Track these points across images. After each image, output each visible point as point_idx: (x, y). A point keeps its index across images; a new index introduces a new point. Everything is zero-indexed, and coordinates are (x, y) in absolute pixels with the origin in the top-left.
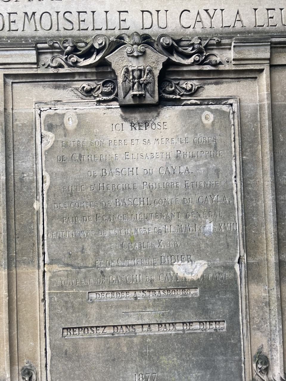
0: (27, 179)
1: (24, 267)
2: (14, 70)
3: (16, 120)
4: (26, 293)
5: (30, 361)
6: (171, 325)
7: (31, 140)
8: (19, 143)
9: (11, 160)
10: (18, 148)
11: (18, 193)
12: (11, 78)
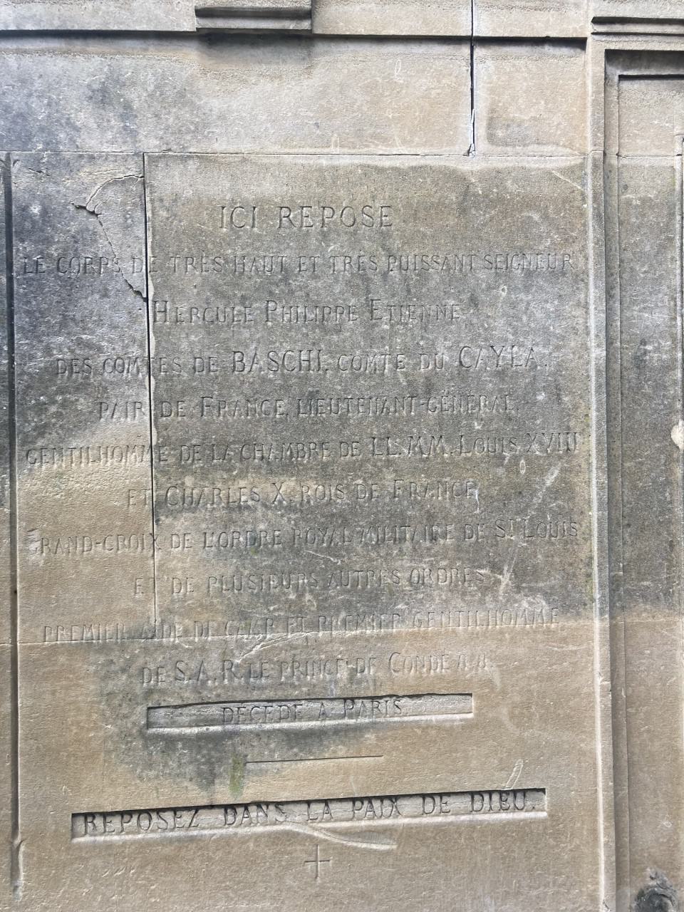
0: (654, 358)
1: (645, 610)
2: (635, 38)
3: (626, 187)
4: (650, 683)
5: (660, 872)
6: (519, 795)
7: (665, 248)
8: (634, 254)
9: (614, 303)
10: (631, 268)
11: (630, 399)
12: (619, 63)
